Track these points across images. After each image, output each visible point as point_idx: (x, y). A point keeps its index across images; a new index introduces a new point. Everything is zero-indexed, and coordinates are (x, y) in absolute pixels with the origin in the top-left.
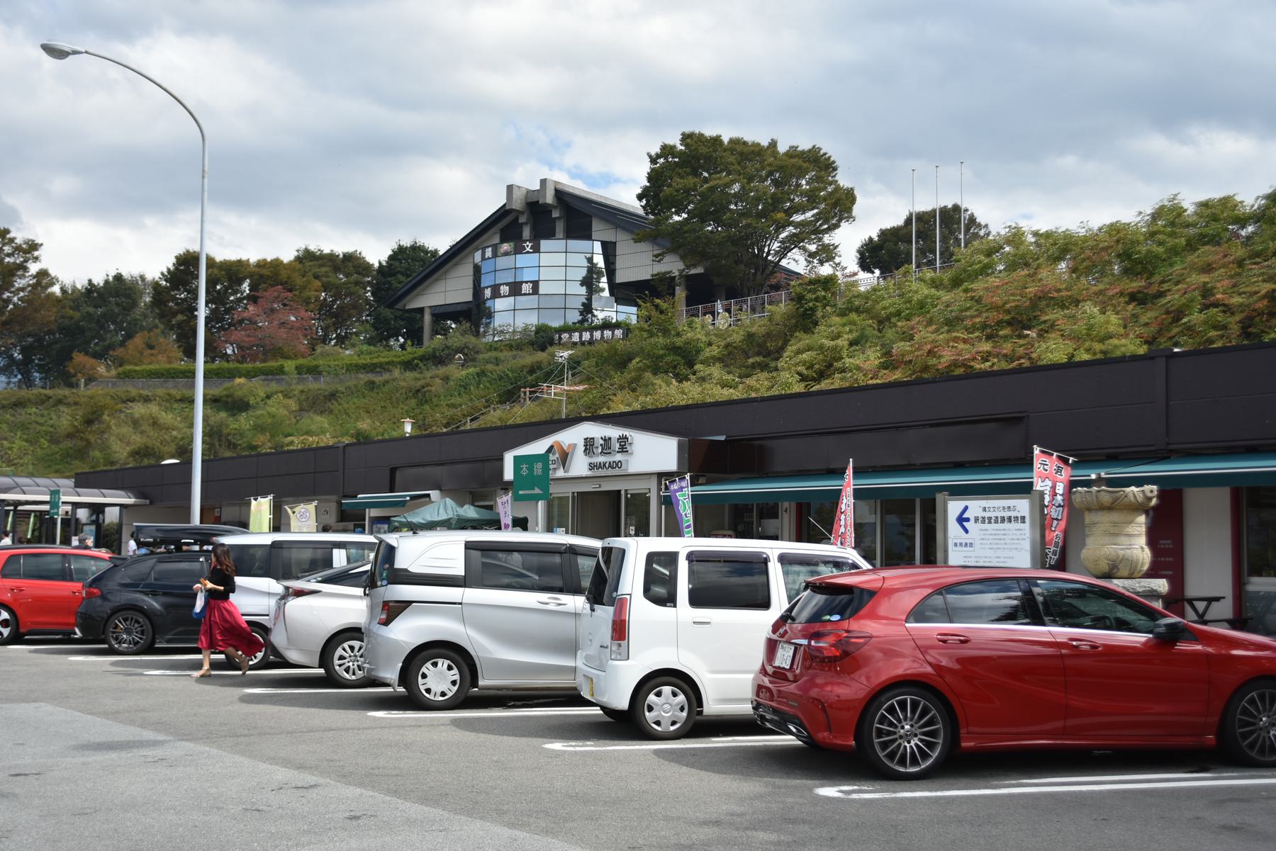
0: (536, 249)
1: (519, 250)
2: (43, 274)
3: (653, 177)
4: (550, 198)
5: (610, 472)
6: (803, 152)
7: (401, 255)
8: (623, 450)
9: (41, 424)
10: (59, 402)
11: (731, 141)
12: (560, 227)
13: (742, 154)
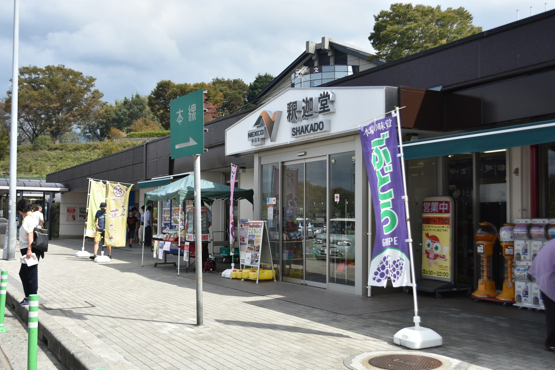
0: (320, 71)
1: (312, 72)
2: (96, 92)
3: (378, 28)
4: (327, 47)
5: (312, 136)
6: (455, 10)
7: (259, 79)
8: (325, 109)
9: (87, 158)
10: (95, 148)
11: (417, 6)
12: (332, 60)
13: (422, 12)
